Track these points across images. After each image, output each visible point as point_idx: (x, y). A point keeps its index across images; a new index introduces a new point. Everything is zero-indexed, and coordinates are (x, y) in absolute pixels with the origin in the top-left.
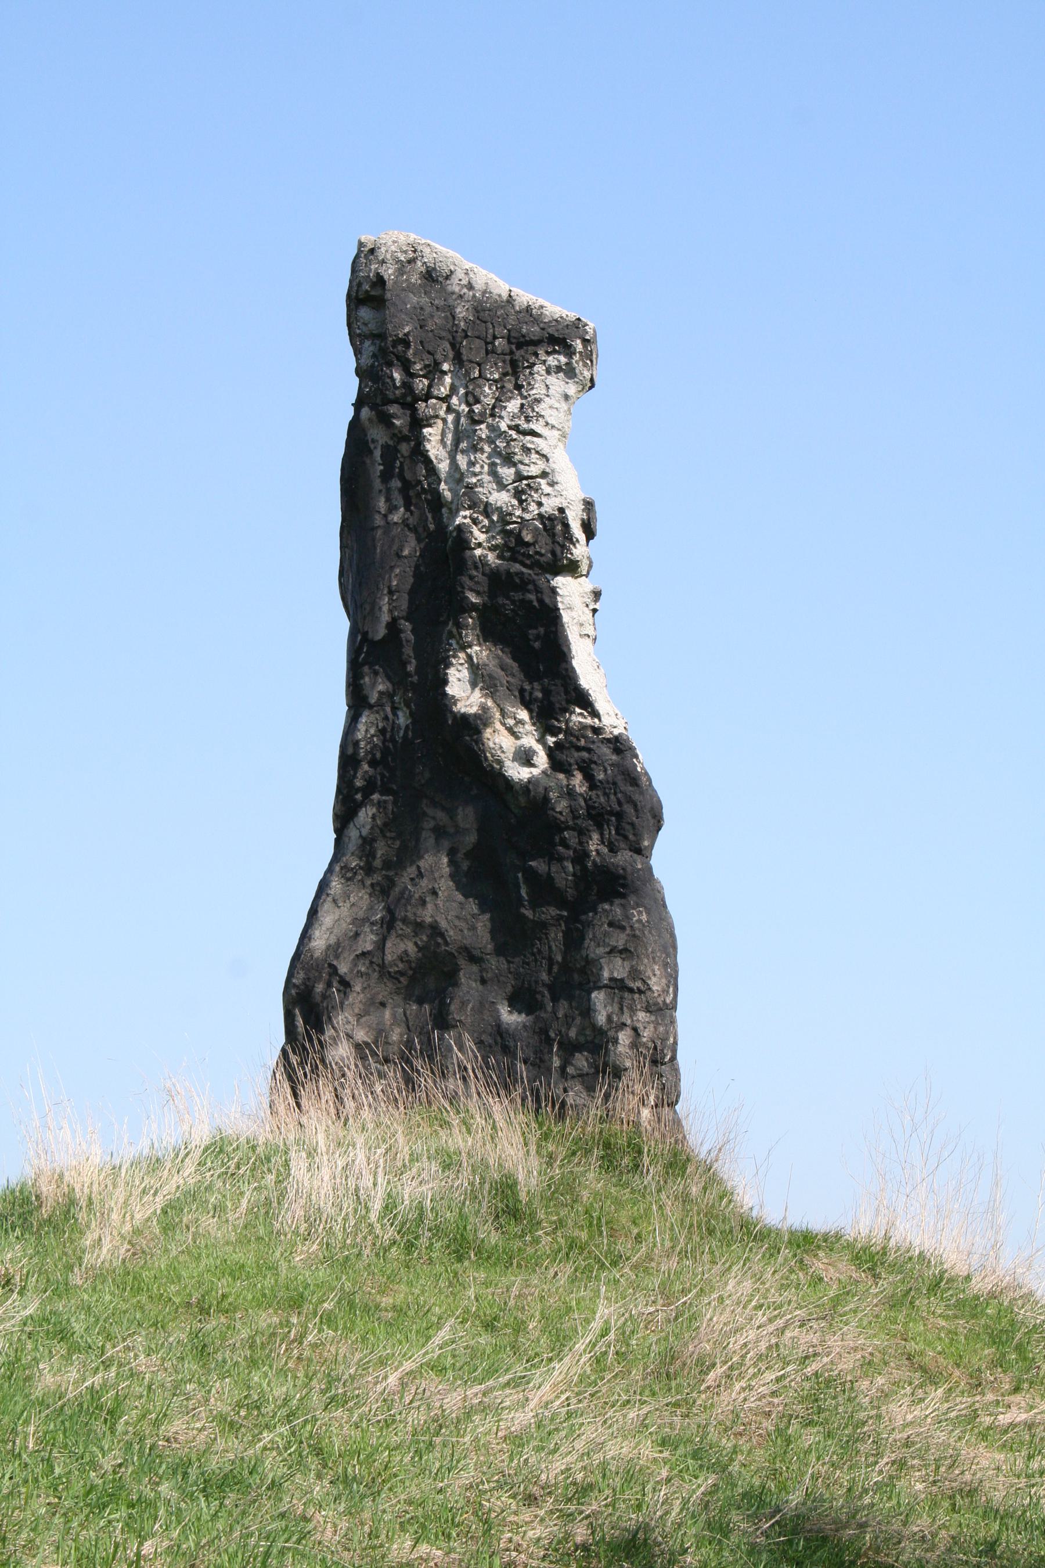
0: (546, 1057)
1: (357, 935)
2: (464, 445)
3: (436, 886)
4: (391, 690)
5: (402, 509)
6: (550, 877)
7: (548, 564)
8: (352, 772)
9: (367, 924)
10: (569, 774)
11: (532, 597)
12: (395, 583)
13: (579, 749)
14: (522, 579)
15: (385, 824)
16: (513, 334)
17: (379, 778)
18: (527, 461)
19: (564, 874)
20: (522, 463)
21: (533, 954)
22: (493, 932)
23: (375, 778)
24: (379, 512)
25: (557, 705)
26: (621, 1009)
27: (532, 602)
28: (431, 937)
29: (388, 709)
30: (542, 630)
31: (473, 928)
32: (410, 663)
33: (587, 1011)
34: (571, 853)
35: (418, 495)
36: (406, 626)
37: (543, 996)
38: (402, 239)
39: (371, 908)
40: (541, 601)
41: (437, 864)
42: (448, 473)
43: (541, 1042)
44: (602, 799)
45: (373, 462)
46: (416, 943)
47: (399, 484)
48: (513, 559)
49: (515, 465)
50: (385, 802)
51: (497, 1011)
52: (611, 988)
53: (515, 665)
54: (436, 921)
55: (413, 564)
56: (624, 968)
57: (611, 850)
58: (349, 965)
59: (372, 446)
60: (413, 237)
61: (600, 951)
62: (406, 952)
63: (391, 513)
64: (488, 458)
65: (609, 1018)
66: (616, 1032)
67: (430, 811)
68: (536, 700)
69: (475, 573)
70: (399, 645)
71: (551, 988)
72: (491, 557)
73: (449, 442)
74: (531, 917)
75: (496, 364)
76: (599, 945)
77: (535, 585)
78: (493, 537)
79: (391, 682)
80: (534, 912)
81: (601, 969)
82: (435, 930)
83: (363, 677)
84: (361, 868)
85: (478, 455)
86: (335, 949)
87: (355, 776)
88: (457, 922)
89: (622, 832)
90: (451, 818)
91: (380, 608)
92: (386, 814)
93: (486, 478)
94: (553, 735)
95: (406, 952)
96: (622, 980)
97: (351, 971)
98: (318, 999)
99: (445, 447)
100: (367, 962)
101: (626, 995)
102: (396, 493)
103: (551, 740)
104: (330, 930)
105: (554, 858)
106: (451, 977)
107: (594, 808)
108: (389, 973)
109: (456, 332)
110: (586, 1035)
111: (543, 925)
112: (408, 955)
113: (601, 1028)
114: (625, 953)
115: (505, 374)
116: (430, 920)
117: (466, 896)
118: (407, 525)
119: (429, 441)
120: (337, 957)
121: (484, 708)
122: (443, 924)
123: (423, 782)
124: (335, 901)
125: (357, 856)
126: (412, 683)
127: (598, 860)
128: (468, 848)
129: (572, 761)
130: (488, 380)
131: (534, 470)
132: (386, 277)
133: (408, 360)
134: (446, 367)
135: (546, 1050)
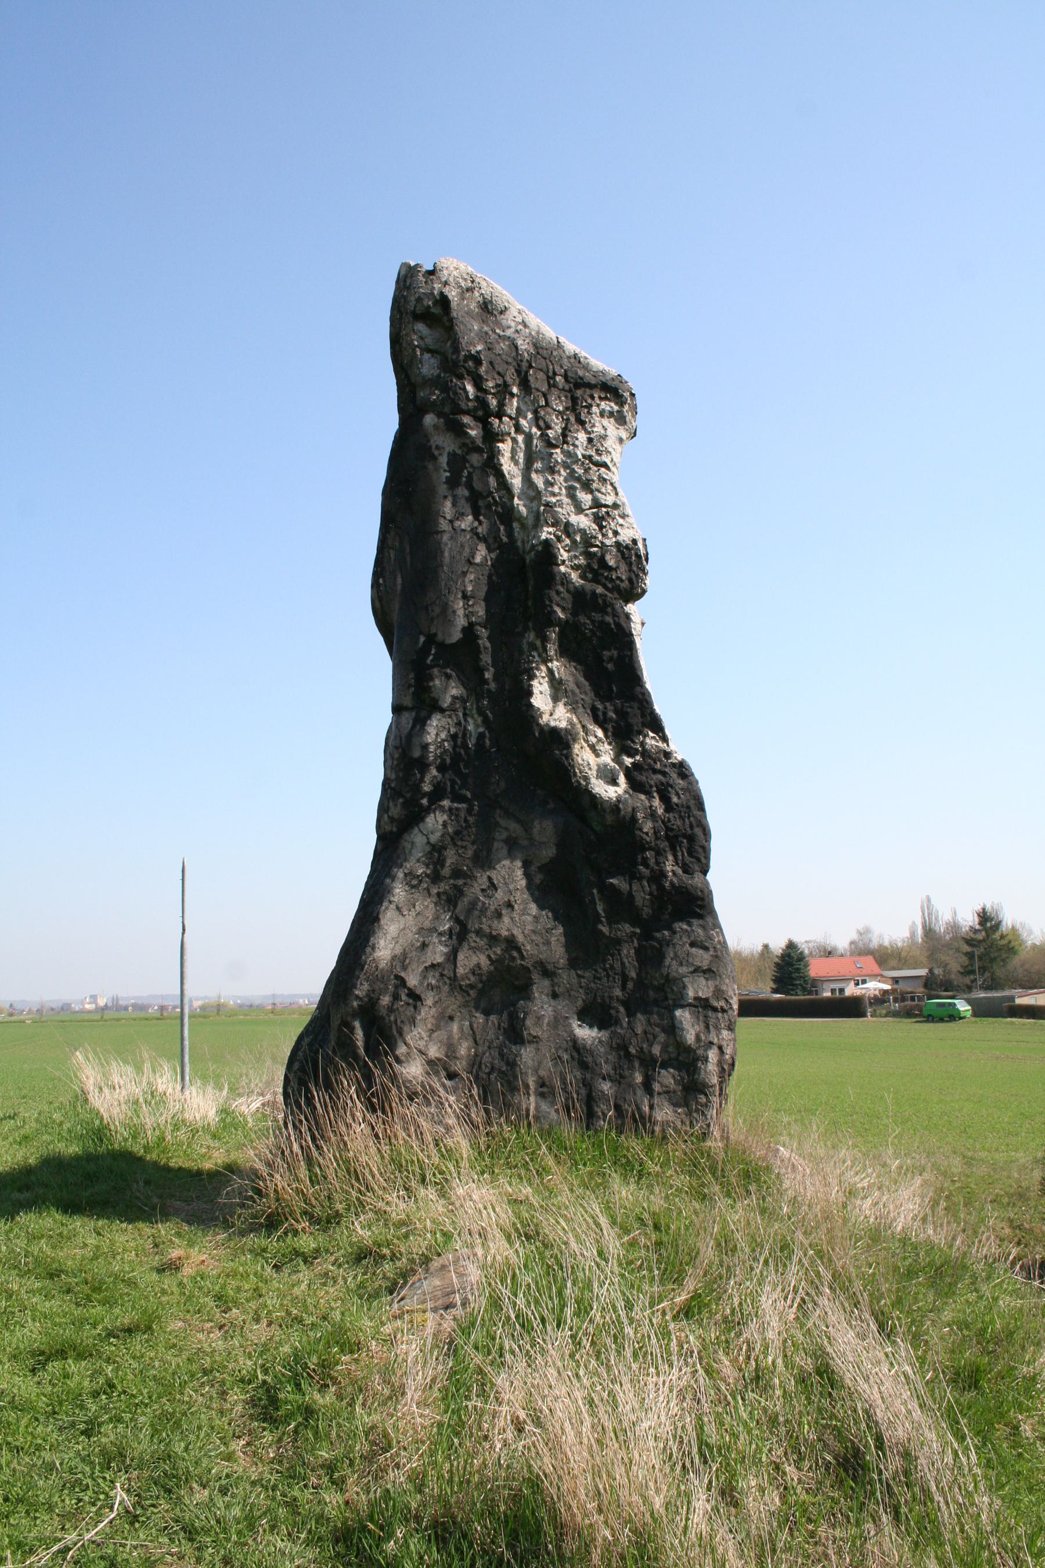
0: (626, 1073)
1: (424, 945)
2: (538, 465)
3: (512, 899)
4: (465, 696)
5: (470, 517)
6: (630, 895)
7: (625, 589)
8: (418, 776)
9: (435, 935)
10: (649, 794)
11: (609, 619)
12: (470, 588)
13: (655, 771)
14: (605, 601)
15: (457, 833)
16: (570, 374)
17: (449, 784)
18: (603, 490)
19: (642, 894)
20: (599, 491)
21: (605, 970)
22: (568, 946)
23: (445, 783)
24: (445, 518)
25: (636, 728)
26: (707, 1027)
27: (609, 624)
28: (505, 950)
29: (461, 714)
30: (615, 653)
31: (548, 943)
32: (488, 670)
33: (672, 1029)
34: (648, 871)
35: (489, 506)
36: (483, 632)
37: (618, 1012)
38: (462, 266)
39: (437, 918)
40: (618, 625)
41: (511, 876)
42: (522, 490)
43: (620, 1057)
44: (679, 822)
45: (437, 469)
46: (489, 957)
47: (466, 493)
48: (596, 580)
49: (591, 492)
50: (457, 809)
51: (570, 1025)
52: (695, 1006)
53: (587, 683)
54: (513, 935)
55: (486, 573)
56: (708, 987)
57: (685, 871)
58: (418, 978)
59: (436, 453)
60: (470, 269)
61: (683, 970)
62: (478, 966)
63: (456, 522)
64: (566, 480)
65: (698, 1038)
66: (706, 1050)
67: (503, 822)
68: (611, 720)
69: (561, 589)
70: (477, 651)
71: (625, 1004)
72: (574, 576)
73: (521, 461)
74: (607, 933)
75: (559, 397)
76: (681, 964)
77: (613, 609)
78: (576, 557)
79: (465, 688)
80: (610, 928)
81: (684, 987)
82: (511, 943)
83: (432, 679)
84: (427, 876)
85: (556, 477)
86: (402, 960)
87: (422, 780)
88: (534, 938)
89: (695, 854)
90: (526, 831)
91: (454, 612)
92: (458, 822)
93: (566, 500)
94: (630, 755)
95: (478, 966)
96: (707, 1000)
97: (421, 983)
98: (384, 1012)
99: (516, 463)
100: (437, 974)
101: (710, 1013)
102: (463, 501)
103: (628, 761)
104: (396, 939)
105: (633, 876)
106: (524, 990)
107: (672, 830)
108: (460, 986)
109: (521, 361)
110: (669, 1053)
111: (618, 942)
112: (480, 968)
113: (689, 1046)
114: (709, 972)
115: (567, 409)
116: (506, 933)
117: (541, 907)
118: (477, 534)
119: (503, 455)
120: (405, 968)
121: (570, 722)
122: (520, 938)
123: (498, 791)
124: (398, 908)
125: (424, 863)
126: (489, 691)
127: (675, 880)
128: (543, 862)
129: (652, 783)
130: (555, 410)
131: (609, 500)
132: (450, 297)
133: (480, 377)
134: (515, 390)
135: (626, 1067)
